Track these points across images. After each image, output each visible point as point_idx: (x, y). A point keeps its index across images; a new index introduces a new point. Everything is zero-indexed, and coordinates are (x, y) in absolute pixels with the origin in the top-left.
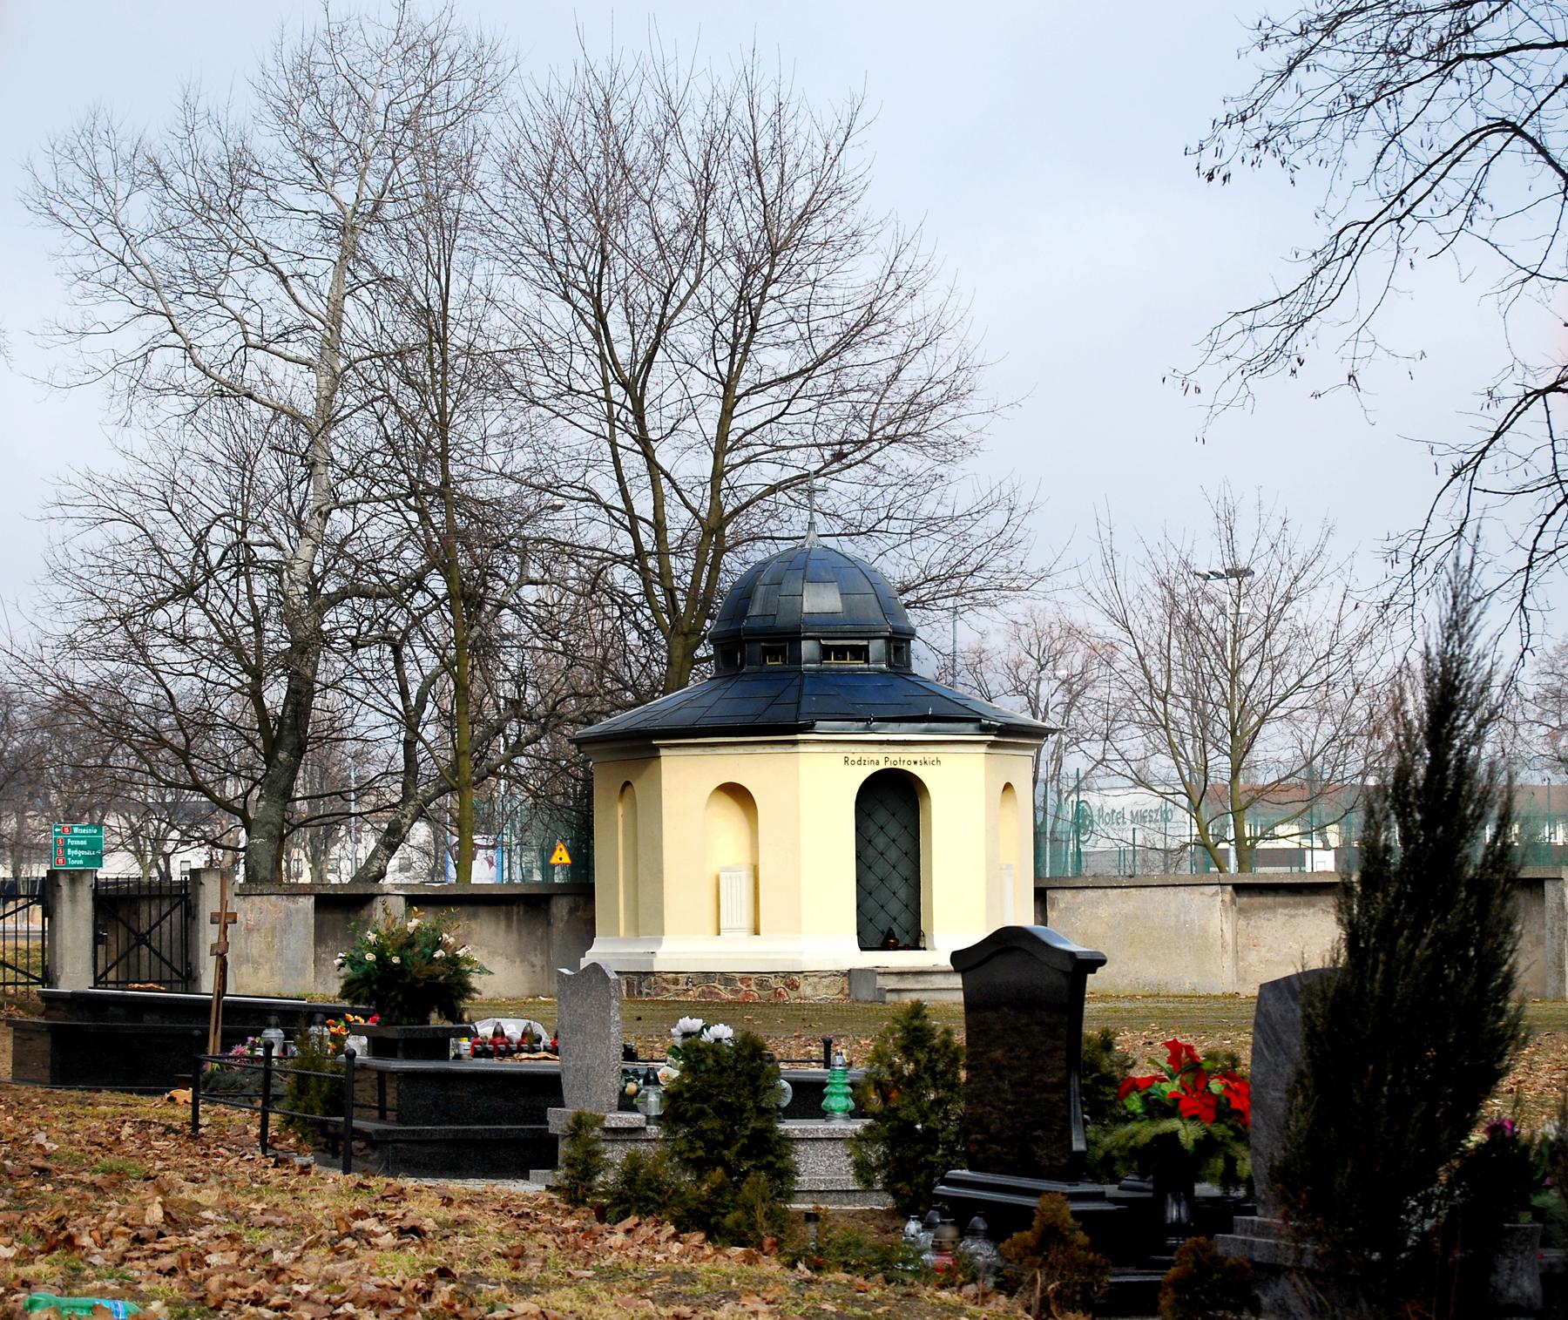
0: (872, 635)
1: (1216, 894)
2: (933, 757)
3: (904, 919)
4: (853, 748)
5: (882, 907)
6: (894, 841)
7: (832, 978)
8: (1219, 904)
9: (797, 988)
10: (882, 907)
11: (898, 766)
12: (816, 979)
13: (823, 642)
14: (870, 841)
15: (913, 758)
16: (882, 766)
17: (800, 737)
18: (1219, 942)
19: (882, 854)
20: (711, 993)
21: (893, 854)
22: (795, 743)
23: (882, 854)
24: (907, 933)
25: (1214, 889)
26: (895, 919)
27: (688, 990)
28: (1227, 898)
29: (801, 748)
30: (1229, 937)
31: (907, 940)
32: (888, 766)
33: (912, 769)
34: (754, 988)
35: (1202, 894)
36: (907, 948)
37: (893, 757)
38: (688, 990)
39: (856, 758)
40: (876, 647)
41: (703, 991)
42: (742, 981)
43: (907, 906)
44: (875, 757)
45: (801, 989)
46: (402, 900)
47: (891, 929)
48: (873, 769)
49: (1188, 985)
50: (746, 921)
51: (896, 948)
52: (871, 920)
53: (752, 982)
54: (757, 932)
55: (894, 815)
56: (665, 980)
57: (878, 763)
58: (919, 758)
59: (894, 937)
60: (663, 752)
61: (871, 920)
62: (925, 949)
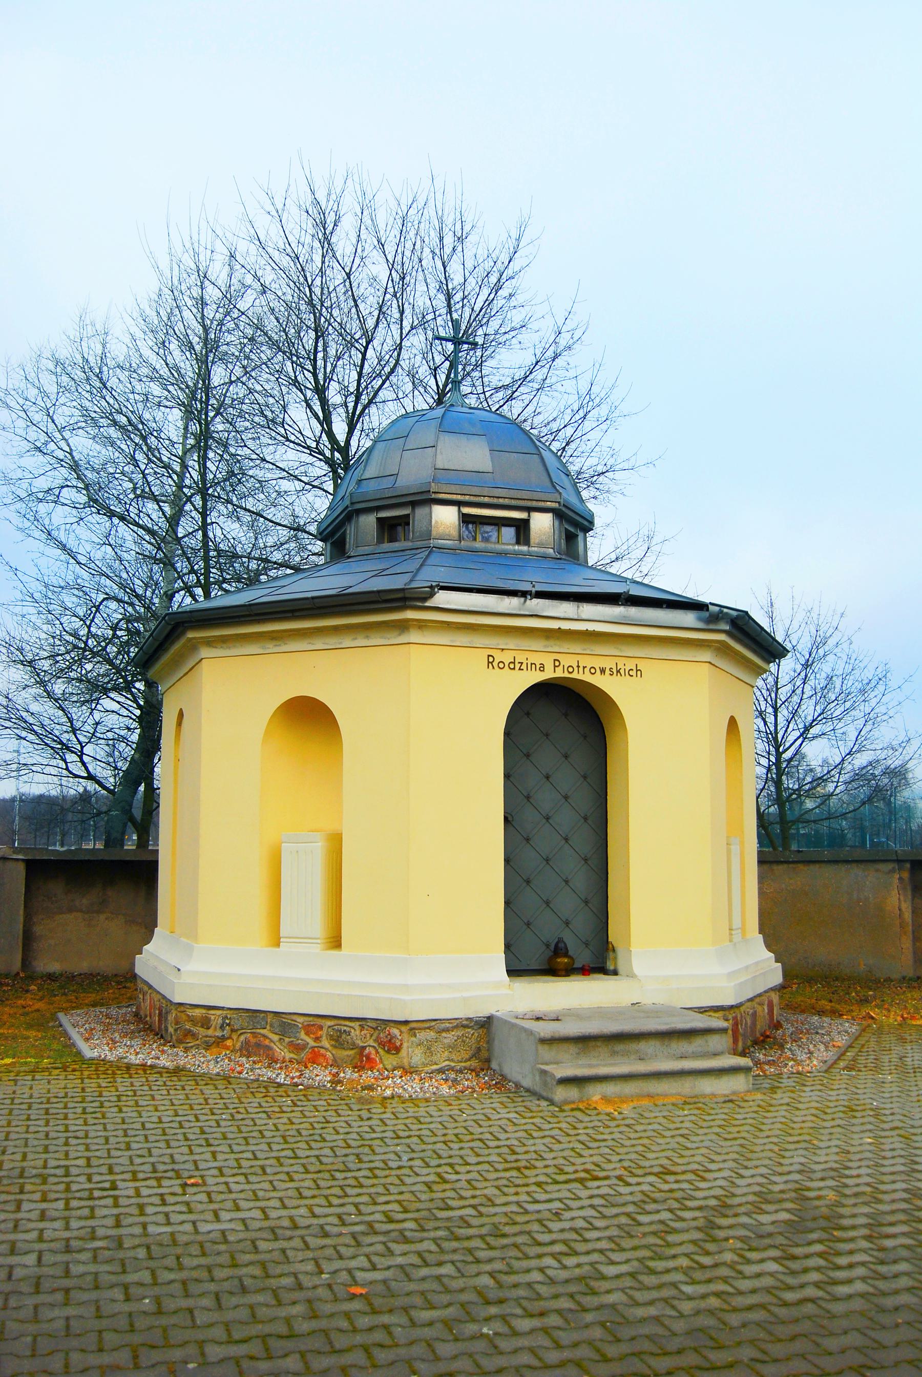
0: (534, 504)
1: (892, 871)
2: (631, 664)
3: (582, 923)
4: (502, 642)
5: (547, 903)
6: (566, 798)
7: (460, 1033)
8: (896, 881)
9: (398, 1050)
10: (547, 903)
11: (575, 675)
12: (432, 1034)
13: (466, 510)
14: (528, 798)
15: (598, 663)
16: (548, 674)
17: (410, 615)
18: (898, 922)
19: (547, 818)
20: (258, 1045)
21: (566, 818)
22: (403, 626)
23: (547, 818)
24: (587, 944)
25: (890, 866)
26: (567, 923)
27: (223, 1038)
28: (906, 875)
29: (414, 636)
30: (908, 916)
31: (583, 957)
32: (559, 673)
33: (598, 681)
34: (325, 1043)
35: (877, 870)
36: (586, 971)
37: (566, 661)
38: (223, 1038)
39: (507, 657)
40: (542, 524)
41: (247, 1042)
42: (308, 1029)
43: (586, 902)
44: (537, 659)
45: (403, 1053)
46: (22, 867)
47: (560, 940)
48: (537, 677)
49: (862, 967)
50: (317, 926)
51: (568, 971)
52: (528, 924)
53: (324, 1033)
54: (336, 942)
55: (566, 757)
56: (192, 1020)
57: (542, 668)
58: (608, 663)
59: (566, 955)
60: (205, 652)
61: (528, 924)
62: (615, 973)
